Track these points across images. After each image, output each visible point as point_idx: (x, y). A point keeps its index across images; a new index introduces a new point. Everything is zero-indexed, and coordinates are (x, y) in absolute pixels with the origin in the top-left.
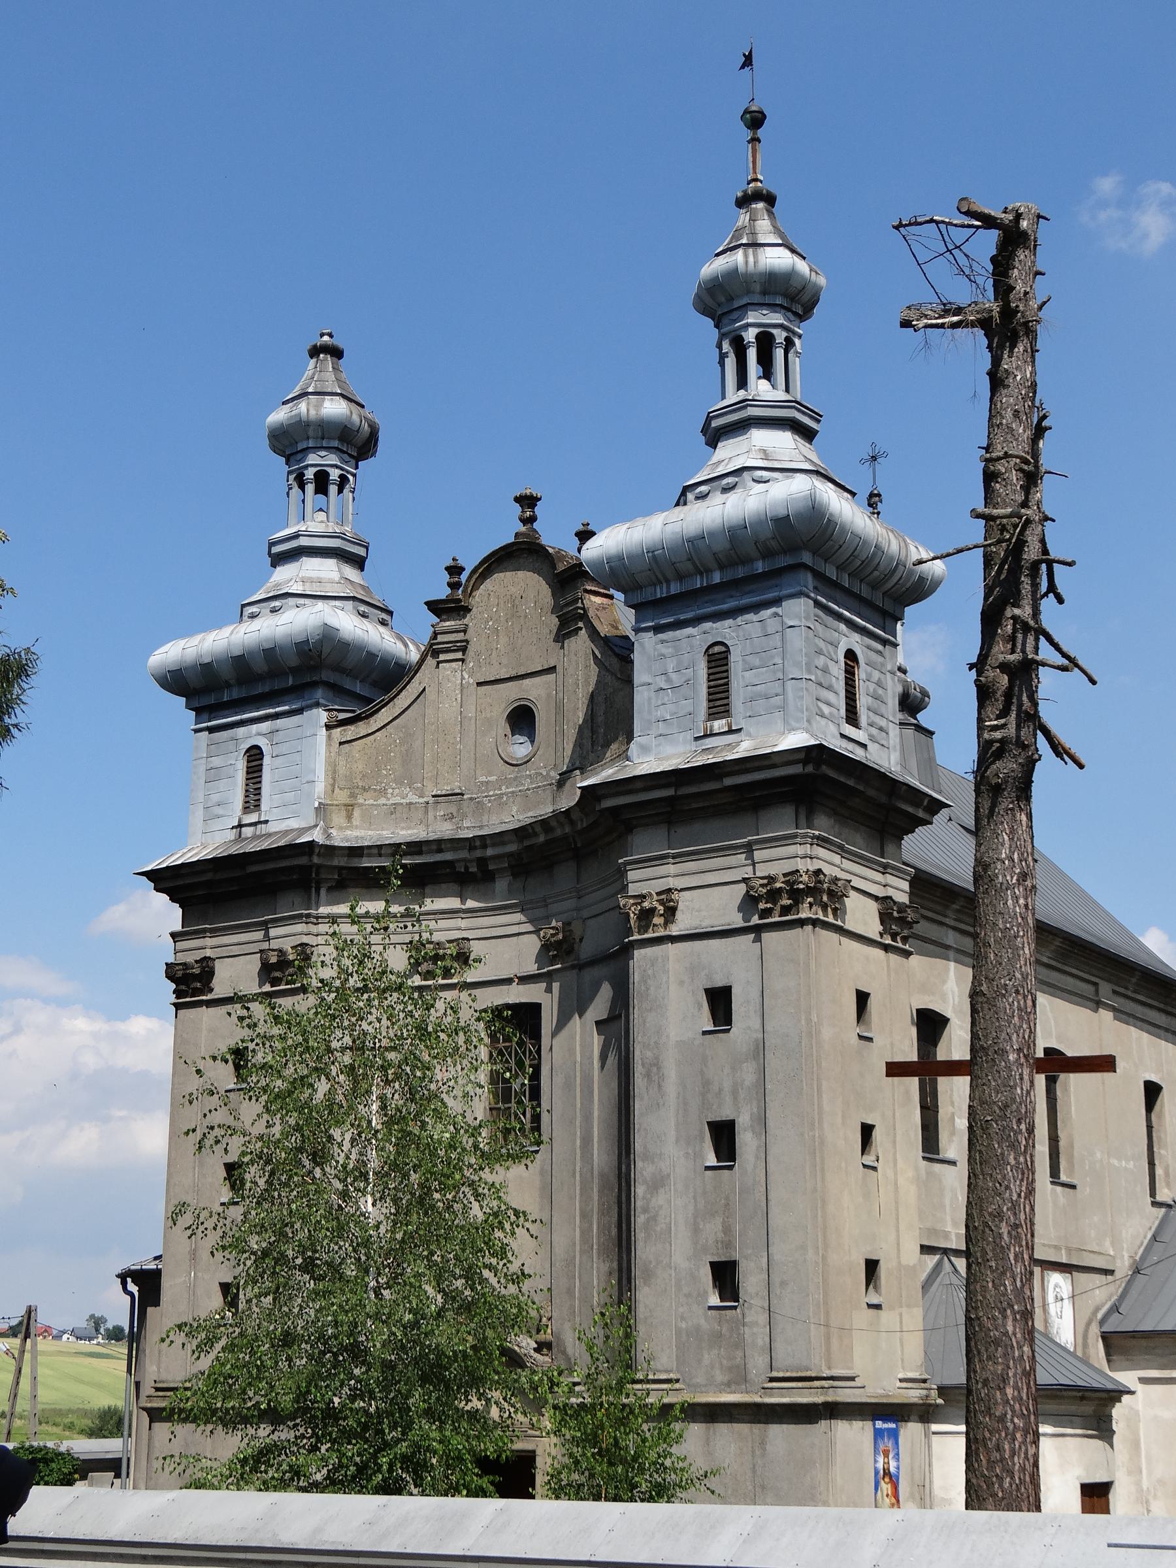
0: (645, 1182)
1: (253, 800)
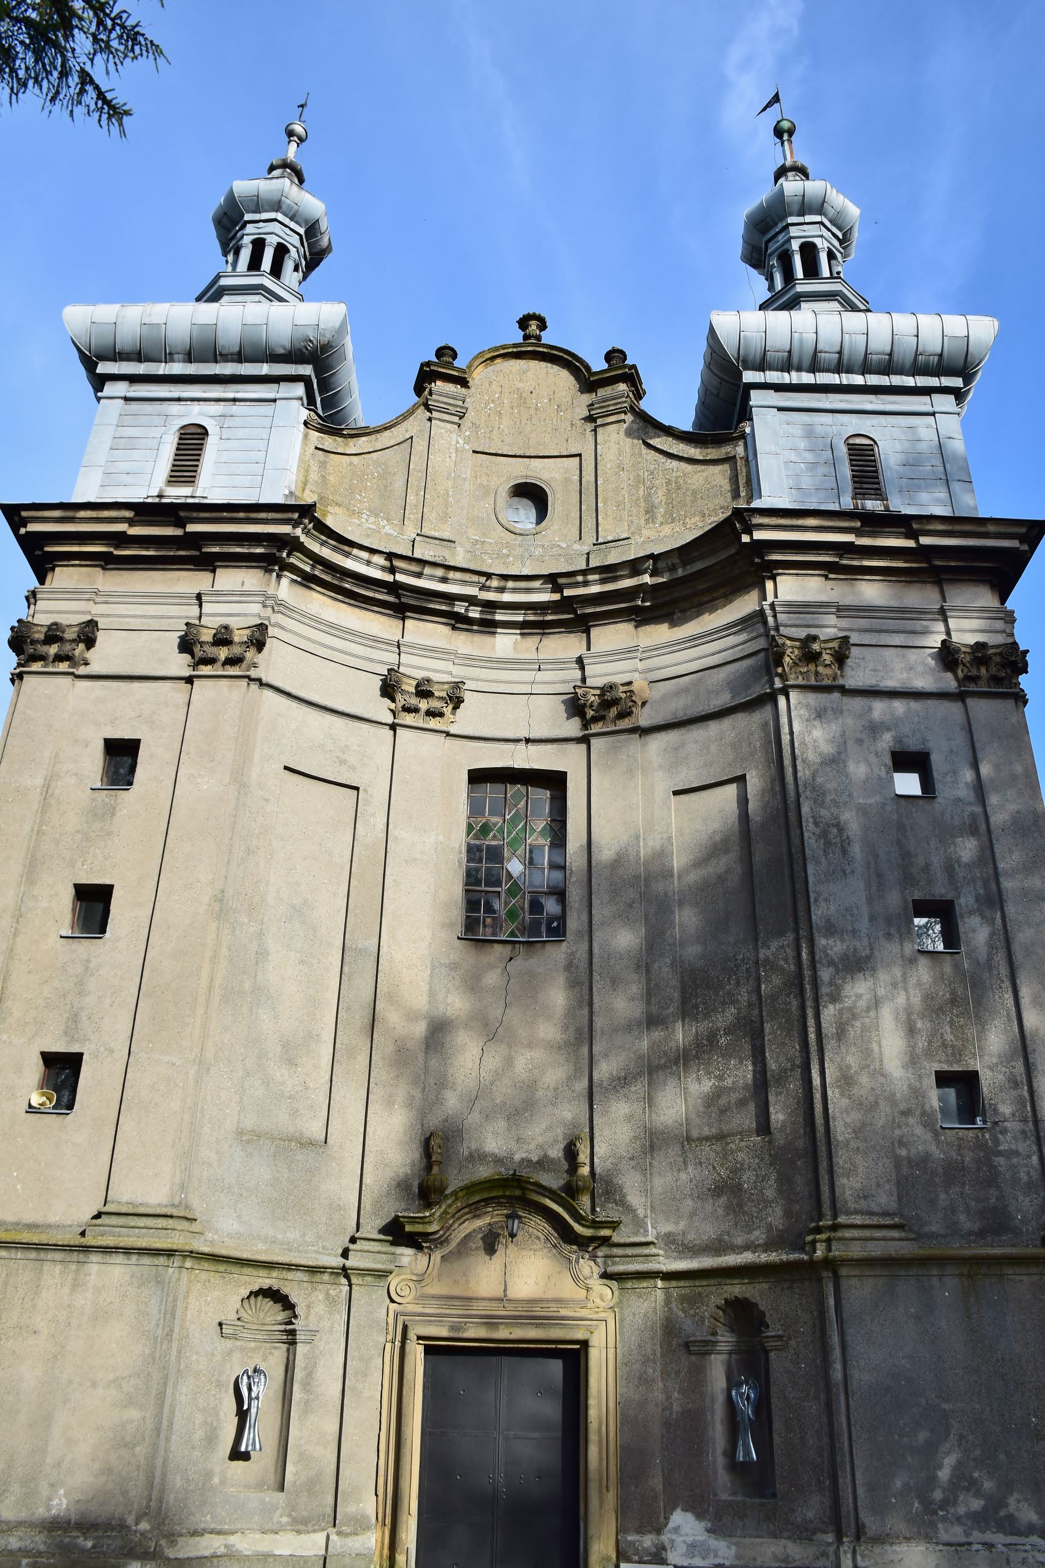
0: (831, 963)
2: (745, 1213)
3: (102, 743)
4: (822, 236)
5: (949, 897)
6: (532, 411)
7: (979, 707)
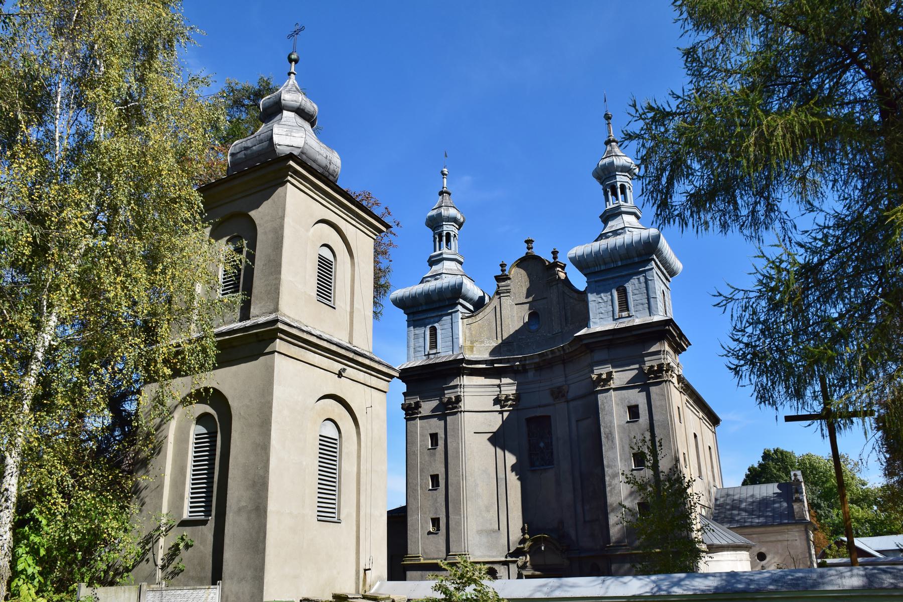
1: (434, 345)
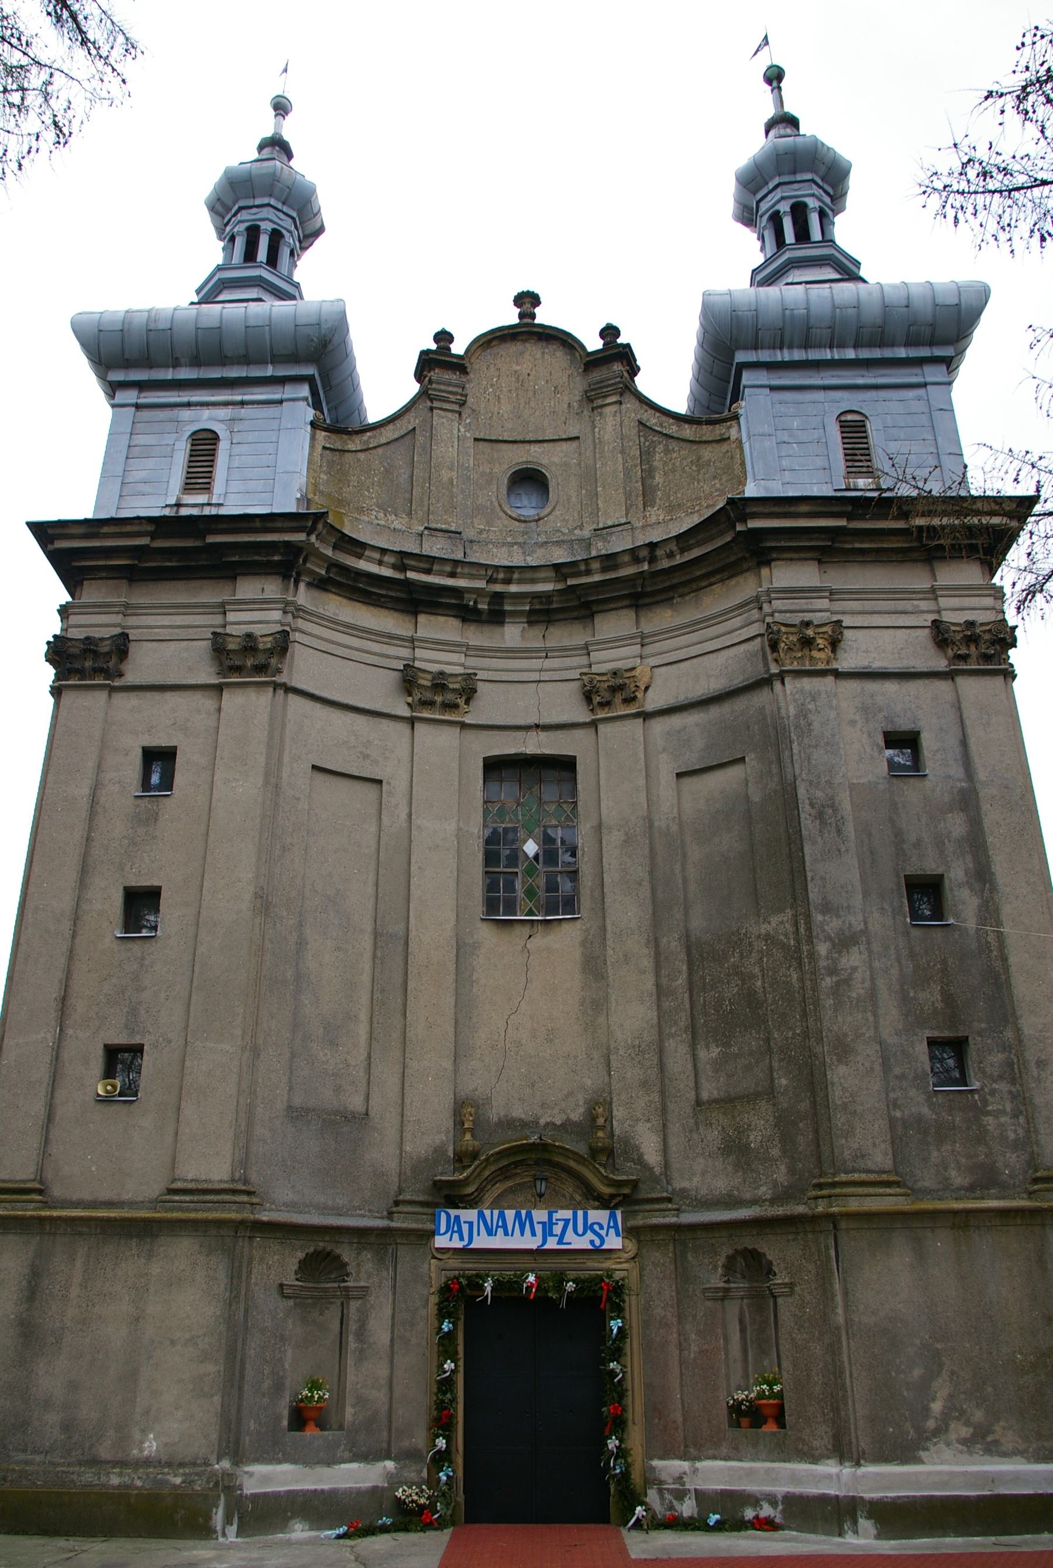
0: (829, 938)
2: (752, 1170)
3: (140, 750)
4: (813, 195)
5: (939, 871)
6: (530, 394)
7: (969, 687)
